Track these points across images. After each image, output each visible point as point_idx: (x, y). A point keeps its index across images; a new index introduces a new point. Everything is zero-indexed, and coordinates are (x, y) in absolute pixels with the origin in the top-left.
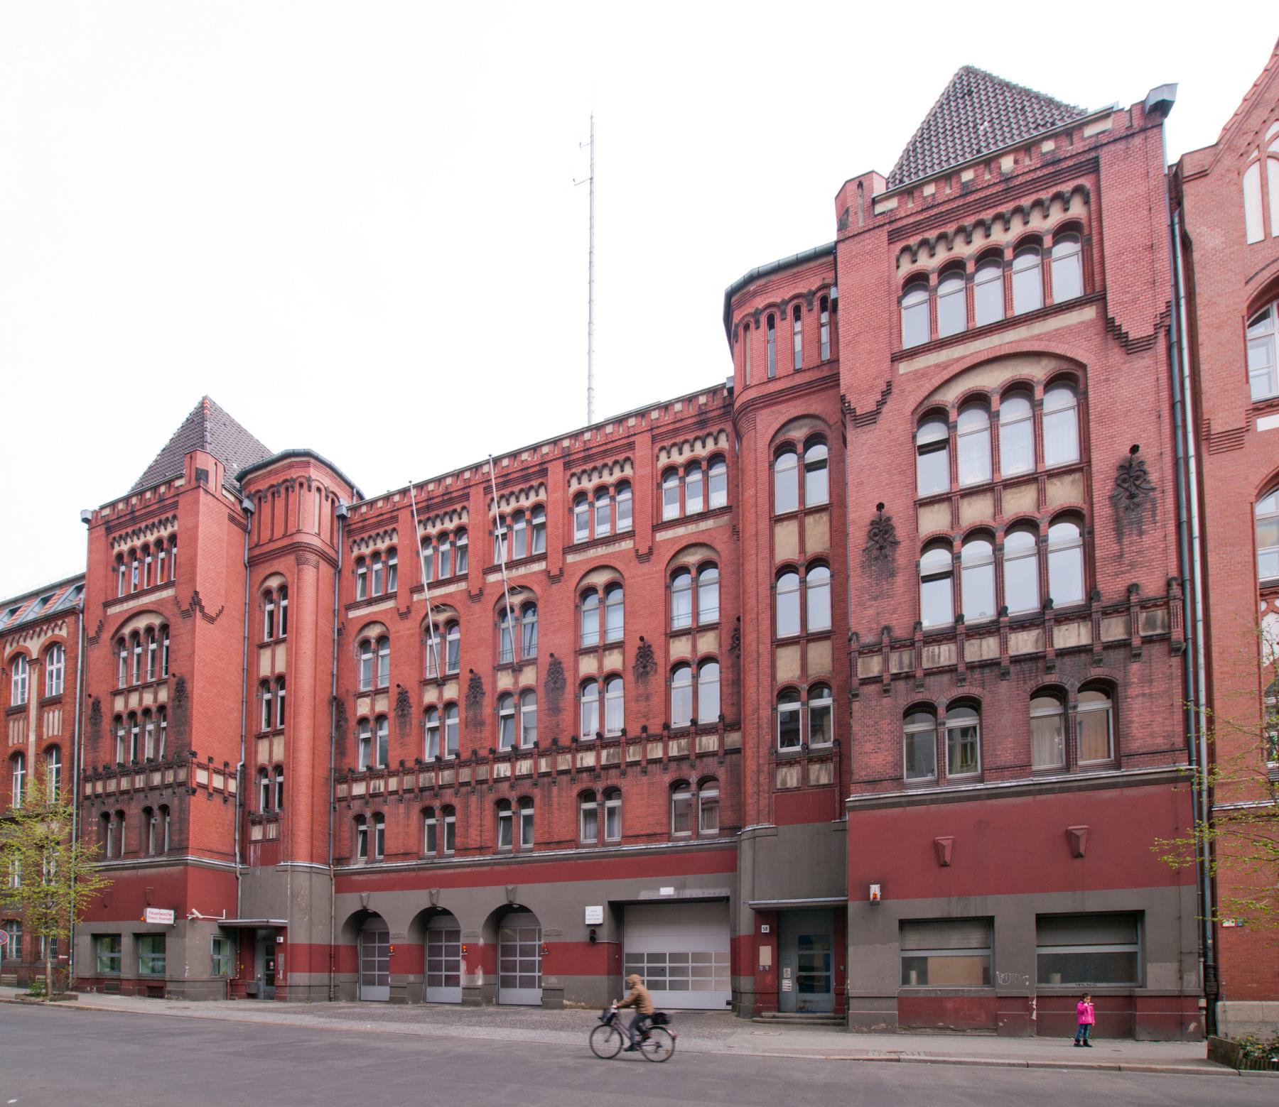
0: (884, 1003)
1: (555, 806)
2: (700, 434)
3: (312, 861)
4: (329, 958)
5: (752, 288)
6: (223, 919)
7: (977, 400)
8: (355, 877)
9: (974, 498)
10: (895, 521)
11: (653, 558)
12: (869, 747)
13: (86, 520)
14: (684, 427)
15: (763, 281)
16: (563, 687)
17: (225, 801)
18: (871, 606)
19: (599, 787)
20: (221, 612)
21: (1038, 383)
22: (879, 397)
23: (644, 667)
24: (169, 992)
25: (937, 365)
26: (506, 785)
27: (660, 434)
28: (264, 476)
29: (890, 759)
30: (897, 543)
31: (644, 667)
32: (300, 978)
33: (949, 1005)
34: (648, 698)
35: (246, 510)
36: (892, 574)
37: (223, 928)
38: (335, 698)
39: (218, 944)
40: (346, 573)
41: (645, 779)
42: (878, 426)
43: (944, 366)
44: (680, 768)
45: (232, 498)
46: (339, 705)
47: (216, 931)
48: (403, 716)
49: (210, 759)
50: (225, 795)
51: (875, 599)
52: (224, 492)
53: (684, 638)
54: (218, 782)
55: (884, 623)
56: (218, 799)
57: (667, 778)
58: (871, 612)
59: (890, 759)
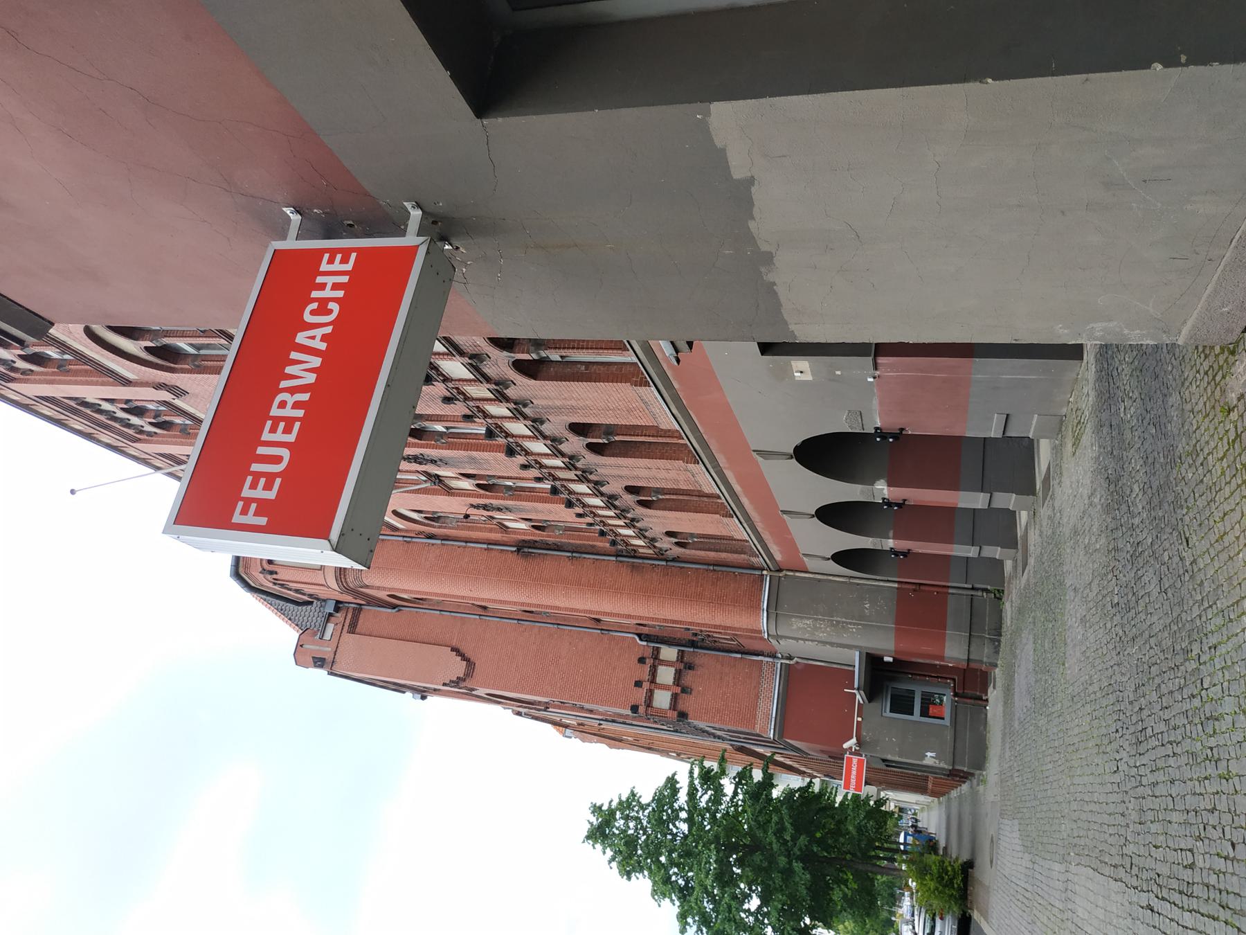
3: (757, 607)
4: (921, 603)
35: (337, 609)
38: (518, 551)
46: (524, 548)
47: (875, 705)
49: (638, 684)
50: (684, 666)
52: (327, 636)
54: (666, 675)
56: (689, 678)
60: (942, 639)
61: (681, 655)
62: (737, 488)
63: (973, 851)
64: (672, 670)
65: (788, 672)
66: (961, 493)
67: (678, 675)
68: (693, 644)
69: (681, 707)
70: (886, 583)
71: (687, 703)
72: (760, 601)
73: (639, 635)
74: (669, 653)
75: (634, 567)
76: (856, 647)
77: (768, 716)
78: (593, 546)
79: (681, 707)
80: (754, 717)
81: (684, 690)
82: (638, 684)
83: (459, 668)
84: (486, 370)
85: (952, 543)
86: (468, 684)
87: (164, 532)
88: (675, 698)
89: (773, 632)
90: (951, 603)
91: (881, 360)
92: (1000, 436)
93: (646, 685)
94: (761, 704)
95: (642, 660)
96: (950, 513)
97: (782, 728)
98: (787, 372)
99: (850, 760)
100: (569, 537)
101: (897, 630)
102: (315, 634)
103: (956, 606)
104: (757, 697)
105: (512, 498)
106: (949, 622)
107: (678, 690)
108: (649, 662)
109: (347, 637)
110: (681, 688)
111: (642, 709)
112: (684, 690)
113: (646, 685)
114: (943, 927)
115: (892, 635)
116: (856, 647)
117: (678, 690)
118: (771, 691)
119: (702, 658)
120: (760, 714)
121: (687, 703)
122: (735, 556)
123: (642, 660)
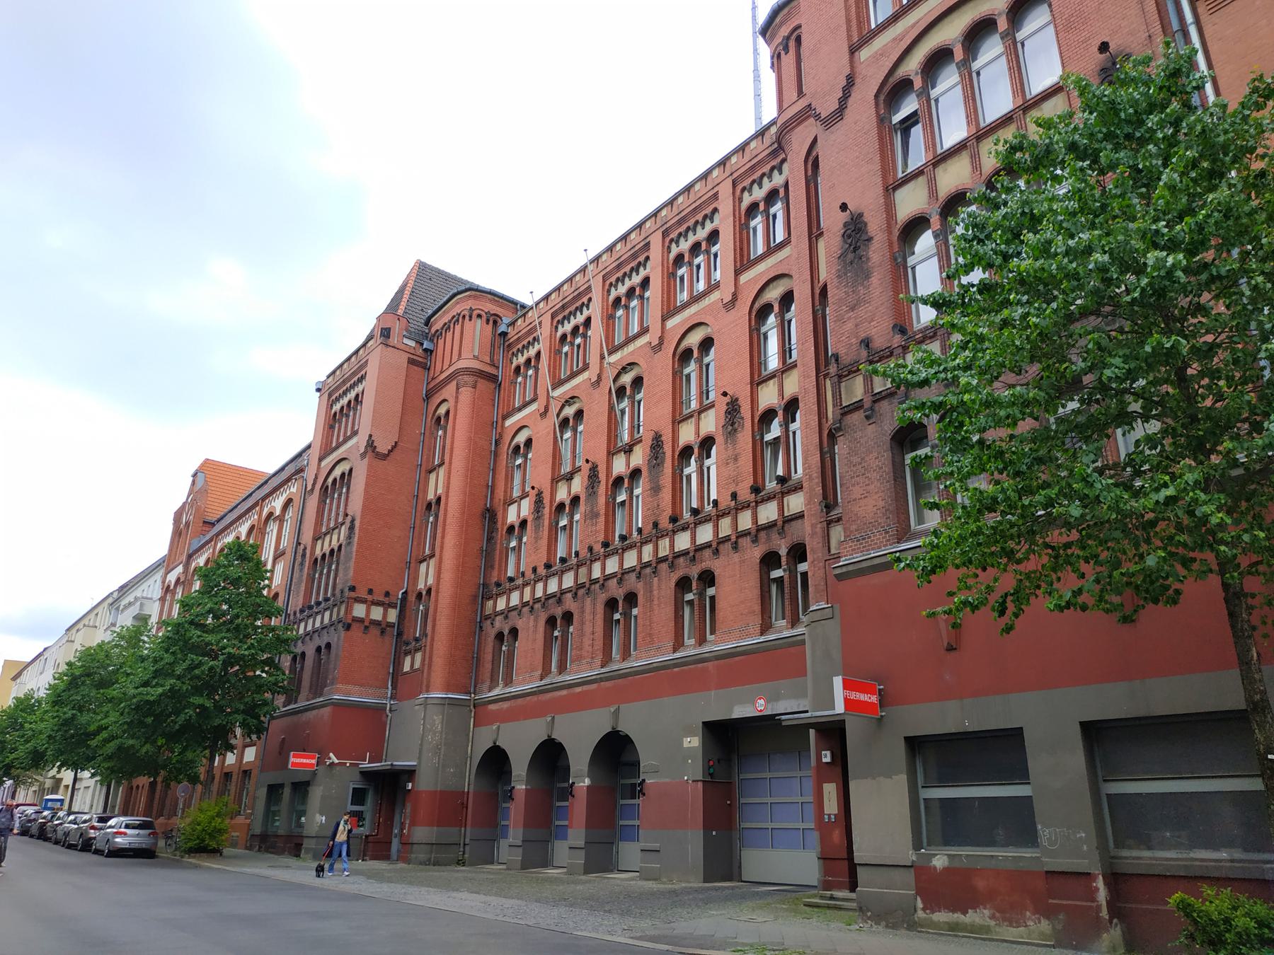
0: (897, 875)
1: (656, 602)
2: (774, 163)
3: (448, 690)
4: (450, 808)
5: (778, 20)
6: (366, 765)
7: (940, 58)
8: (492, 707)
9: (949, 162)
10: (867, 218)
11: (738, 303)
12: (857, 492)
13: (318, 390)
14: (759, 162)
15: (785, 11)
16: (663, 462)
17: (383, 632)
18: (850, 318)
19: (694, 572)
20: (394, 447)
21: (1000, 14)
22: (840, 94)
23: (732, 425)
24: (308, 851)
25: (895, 39)
26: (633, 576)
27: (740, 176)
28: (441, 317)
29: (881, 504)
30: (870, 239)
31: (732, 425)
32: (422, 833)
33: (980, 884)
34: (736, 459)
35: (426, 350)
36: (868, 277)
37: (366, 774)
38: (488, 510)
39: (358, 796)
40: (505, 385)
41: (736, 557)
42: (844, 121)
43: (898, 39)
44: (769, 539)
45: (413, 344)
46: (490, 516)
47: (358, 777)
48: (538, 518)
49: (370, 592)
50: (382, 627)
51: (853, 309)
52: (406, 341)
53: (771, 382)
54: (377, 614)
55: (863, 335)
56: (375, 631)
57: (756, 553)
58: (850, 325)
59: (881, 504)
60: (430, 824)
61: (391, 625)
62: (579, 689)
63: (229, 857)
64: (380, 618)
65: (380, 709)
66: (584, 830)
67: (376, 623)
68: (400, 634)
69: (355, 626)
70: (469, 782)
71: (356, 630)
72: (453, 692)
73: (406, 592)
74: (393, 616)
75: (476, 597)
76: (420, 763)
77: (349, 694)
78: (492, 567)
79: (355, 626)
80: (348, 683)
81: (366, 627)
82: (370, 592)
83: (383, 447)
84: (682, 559)
85: (525, 826)
86: (370, 453)
87: (906, 738)
88: (361, 620)
89: (429, 701)
90: (455, 830)
91: (700, 784)
92: (583, 853)
93: (370, 598)
94: (357, 688)
95: (387, 594)
96: (1102, 809)
97: (338, 705)
98: (691, 733)
99: (313, 758)
100: (501, 553)
101: (436, 792)
102: (407, 330)
103: (452, 833)
104: (362, 685)
105: (550, 524)
106: (441, 829)
107: (367, 623)
108: (386, 600)
109: (405, 357)
110: (367, 625)
111: (353, 594)
112: (366, 627)
113: (370, 598)
114: (132, 836)
115: (431, 788)
116: (420, 763)
117: (367, 623)
118: (367, 696)
119: (389, 642)
120: (349, 687)
121: (356, 630)
122: (488, 675)
123: (387, 594)
